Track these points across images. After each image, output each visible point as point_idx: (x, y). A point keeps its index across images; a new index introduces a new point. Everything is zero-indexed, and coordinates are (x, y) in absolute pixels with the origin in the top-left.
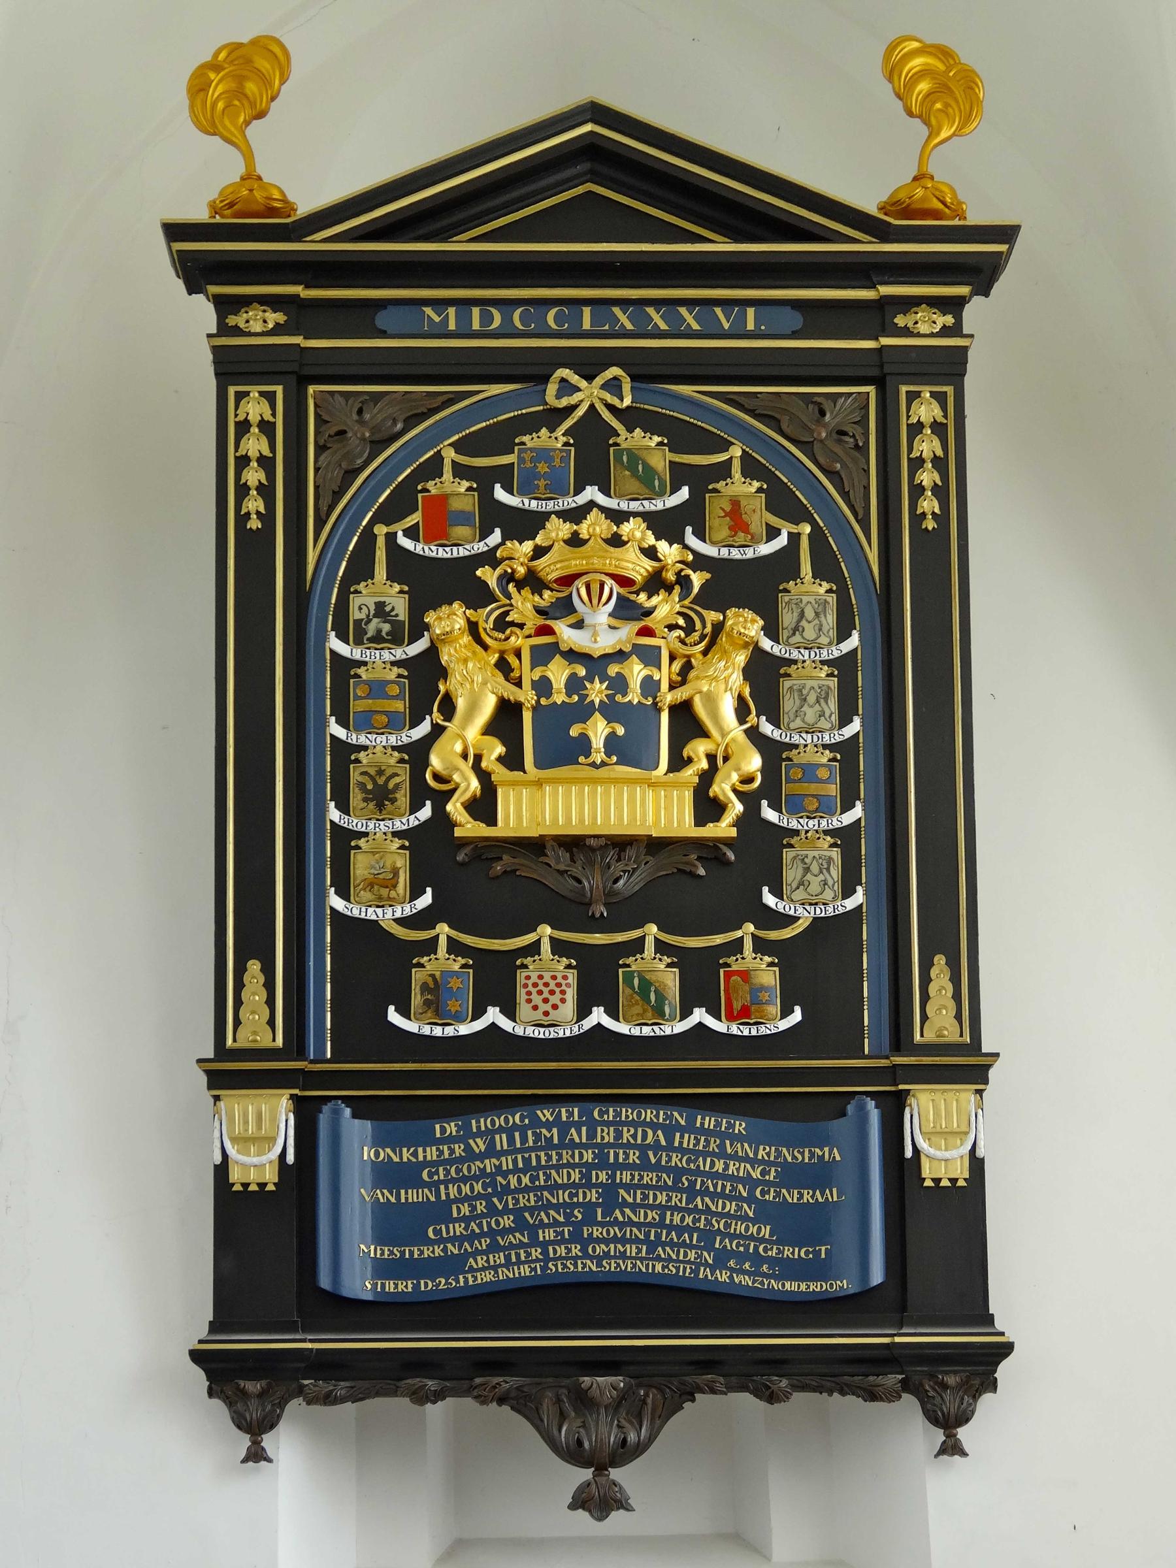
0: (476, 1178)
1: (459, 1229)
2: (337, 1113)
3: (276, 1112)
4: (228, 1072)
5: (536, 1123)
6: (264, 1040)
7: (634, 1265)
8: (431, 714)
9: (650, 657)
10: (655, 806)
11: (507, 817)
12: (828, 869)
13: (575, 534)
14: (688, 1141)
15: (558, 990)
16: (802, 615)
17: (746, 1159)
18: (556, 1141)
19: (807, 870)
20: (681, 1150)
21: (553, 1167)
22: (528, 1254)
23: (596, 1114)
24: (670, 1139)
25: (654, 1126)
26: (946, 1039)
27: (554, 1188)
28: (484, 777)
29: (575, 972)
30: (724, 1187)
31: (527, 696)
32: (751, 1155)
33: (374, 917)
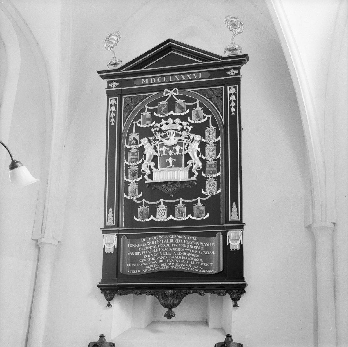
0: (148, 250)
1: (145, 260)
2: (124, 238)
3: (113, 238)
4: (106, 230)
5: (159, 239)
6: (112, 224)
7: (176, 267)
8: (142, 158)
9: (181, 144)
10: (181, 175)
11: (155, 178)
12: (214, 185)
13: (167, 122)
14: (187, 242)
15: (164, 212)
16: (210, 134)
17: (197, 245)
18: (162, 242)
19: (210, 186)
20: (185, 244)
21: (162, 248)
22: (157, 265)
23: (170, 236)
24: (183, 242)
25: (180, 239)
26: (235, 220)
27: (162, 252)
28: (151, 170)
29: (167, 208)
30: (193, 251)
31: (158, 154)
32: (198, 244)
33: (132, 199)
